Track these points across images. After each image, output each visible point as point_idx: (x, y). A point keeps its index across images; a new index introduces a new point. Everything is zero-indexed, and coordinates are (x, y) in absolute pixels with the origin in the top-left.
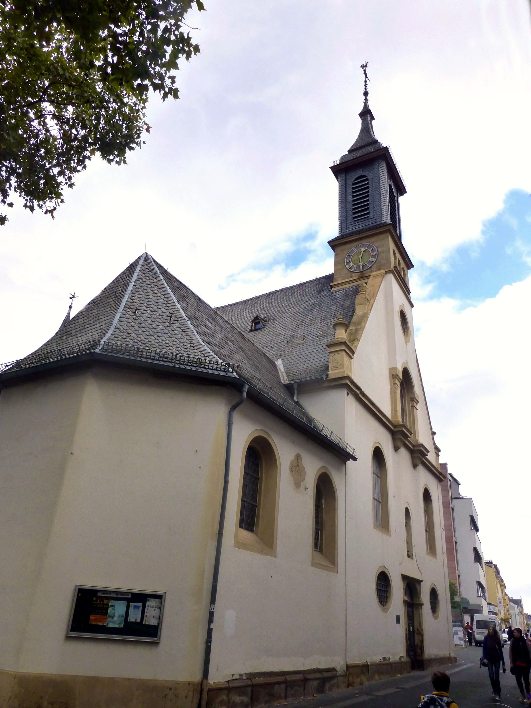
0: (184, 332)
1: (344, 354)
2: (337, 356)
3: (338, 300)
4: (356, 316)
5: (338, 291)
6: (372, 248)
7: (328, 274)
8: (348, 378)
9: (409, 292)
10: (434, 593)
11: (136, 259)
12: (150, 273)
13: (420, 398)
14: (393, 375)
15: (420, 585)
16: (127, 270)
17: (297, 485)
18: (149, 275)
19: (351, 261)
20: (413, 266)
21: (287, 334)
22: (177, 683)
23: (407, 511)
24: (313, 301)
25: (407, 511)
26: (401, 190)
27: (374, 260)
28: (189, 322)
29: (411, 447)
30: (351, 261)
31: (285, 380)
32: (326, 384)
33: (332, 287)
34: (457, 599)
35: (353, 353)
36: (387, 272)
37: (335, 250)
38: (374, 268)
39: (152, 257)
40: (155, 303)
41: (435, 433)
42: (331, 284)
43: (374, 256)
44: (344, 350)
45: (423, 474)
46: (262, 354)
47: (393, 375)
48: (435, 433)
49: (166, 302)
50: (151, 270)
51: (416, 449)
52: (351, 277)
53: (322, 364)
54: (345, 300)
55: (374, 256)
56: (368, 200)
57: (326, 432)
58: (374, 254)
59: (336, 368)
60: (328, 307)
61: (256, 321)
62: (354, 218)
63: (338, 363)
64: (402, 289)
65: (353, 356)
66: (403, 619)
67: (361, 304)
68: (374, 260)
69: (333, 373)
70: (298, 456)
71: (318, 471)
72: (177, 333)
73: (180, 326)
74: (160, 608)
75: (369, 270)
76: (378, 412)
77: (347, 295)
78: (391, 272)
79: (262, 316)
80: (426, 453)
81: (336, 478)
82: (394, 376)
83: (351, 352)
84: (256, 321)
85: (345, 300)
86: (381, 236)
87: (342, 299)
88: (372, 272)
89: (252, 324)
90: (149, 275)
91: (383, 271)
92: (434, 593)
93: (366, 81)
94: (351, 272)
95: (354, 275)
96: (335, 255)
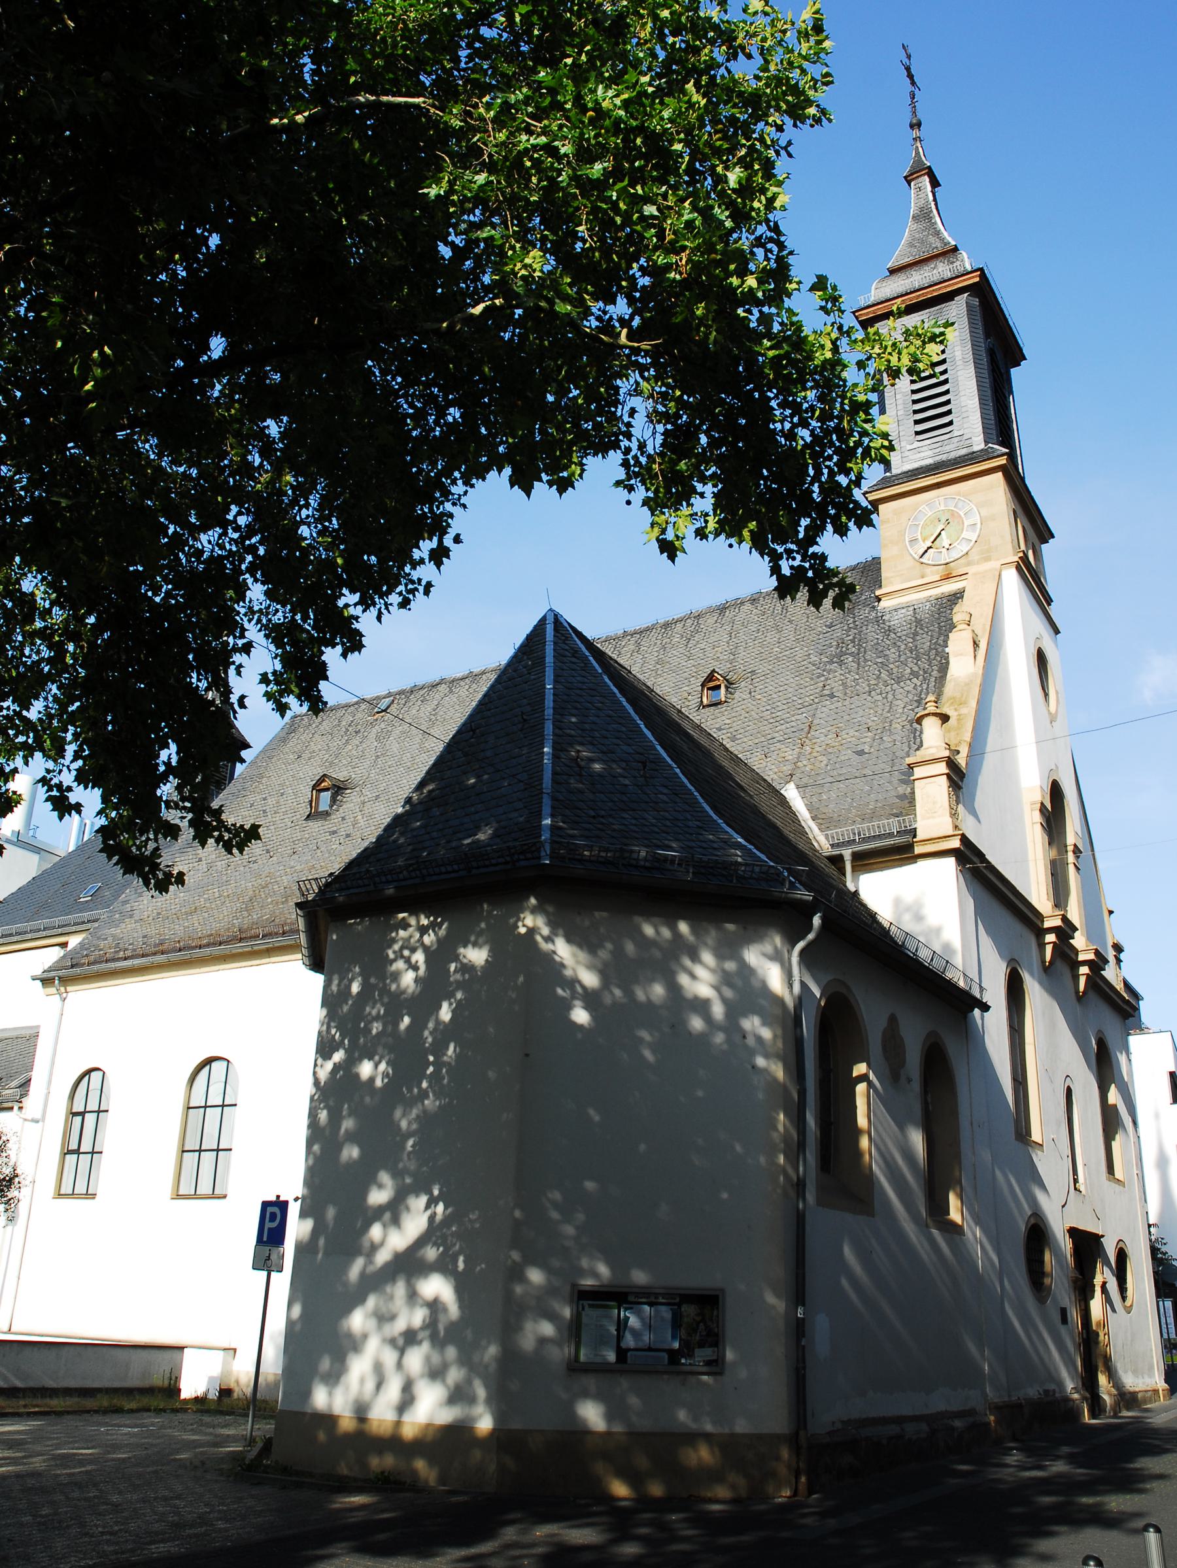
0: (676, 794)
3: (898, 634)
4: (953, 683)
5: (896, 610)
9: (1049, 601)
11: (535, 627)
12: (574, 660)
16: (524, 654)
18: (574, 666)
19: (919, 537)
20: (1052, 536)
21: (793, 719)
26: (1015, 355)
30: (919, 537)
34: (135, 1392)
39: (569, 624)
49: (624, 729)
50: (576, 652)
56: (947, 392)
60: (881, 653)
61: (710, 682)
62: (917, 433)
63: (934, 803)
64: (1031, 591)
65: (962, 781)
67: (961, 655)
70: (893, 1019)
72: (665, 798)
75: (962, 561)
76: (1013, 894)
77: (918, 622)
79: (721, 669)
80: (1070, 932)
81: (952, 1048)
84: (711, 684)
85: (916, 634)
87: (909, 631)
88: (969, 564)
89: (702, 690)
90: (574, 666)
93: (909, 57)
95: (929, 570)
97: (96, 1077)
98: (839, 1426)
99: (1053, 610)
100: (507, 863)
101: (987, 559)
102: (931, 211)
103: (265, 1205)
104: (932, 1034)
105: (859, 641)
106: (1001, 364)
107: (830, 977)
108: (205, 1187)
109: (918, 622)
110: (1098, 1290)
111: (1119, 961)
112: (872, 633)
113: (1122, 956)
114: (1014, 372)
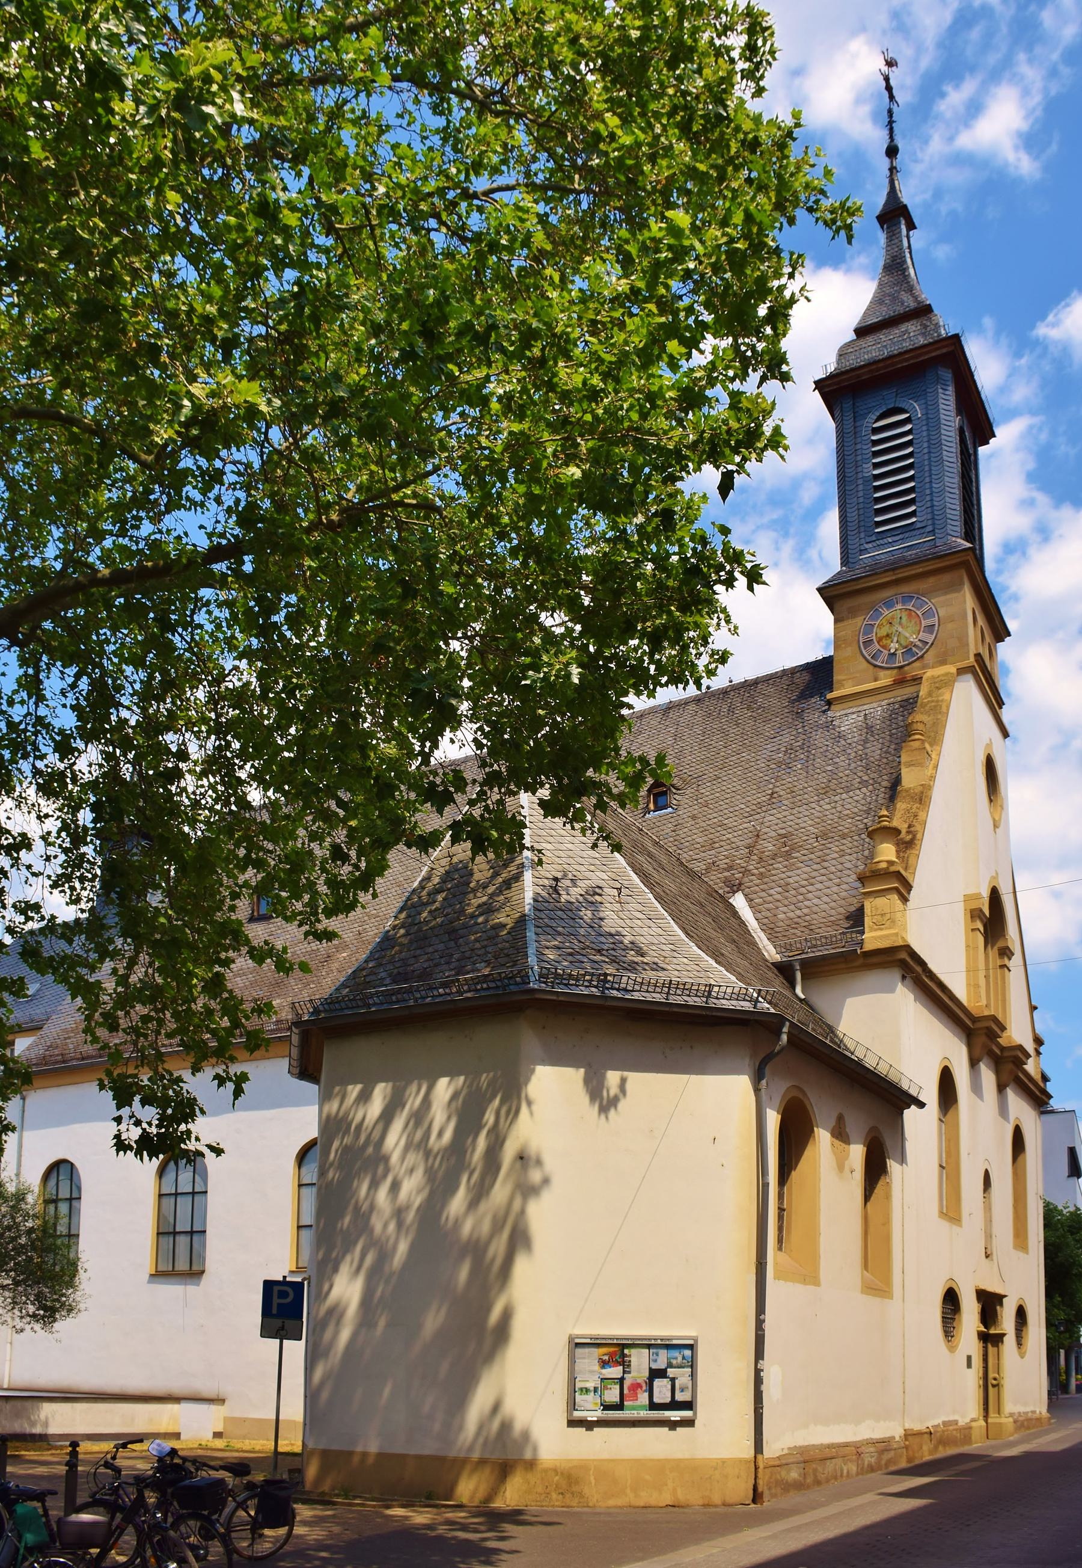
1: (896, 897)
2: (881, 902)
6: (925, 608)
7: (811, 658)
8: (908, 949)
9: (1001, 703)
10: (1021, 1314)
13: (1016, 949)
14: (972, 911)
15: (1001, 1304)
17: (841, 1167)
20: (1009, 635)
22: (724, 1462)
23: (987, 1176)
24: (787, 738)
25: (987, 1176)
27: (930, 638)
28: (651, 896)
29: (998, 1051)
31: (771, 952)
32: (861, 961)
33: (829, 703)
35: (909, 887)
36: (961, 671)
37: (836, 607)
38: (930, 657)
40: (580, 860)
41: (1035, 1008)
42: (829, 696)
43: (930, 628)
44: (896, 889)
45: (1019, 1107)
46: (677, 870)
47: (972, 911)
48: (1035, 1008)
51: (1006, 1054)
52: (876, 680)
53: (841, 910)
54: (866, 741)
55: (930, 628)
57: (870, 1062)
58: (929, 622)
59: (879, 926)
66: (977, 1361)
68: (930, 638)
69: (873, 938)
71: (784, 1096)
73: (640, 908)
74: (692, 1367)
77: (869, 728)
78: (970, 670)
82: (975, 914)
83: (903, 888)
84: (655, 791)
85: (866, 741)
86: (946, 578)
88: (925, 667)
91: (952, 669)
92: (1021, 1314)
94: (875, 666)
96: (836, 621)
97: (63, 1168)
98: (786, 1451)
99: (1006, 714)
100: (497, 987)
101: (943, 662)
102: (905, 262)
103: (194, 1273)
104: (873, 1129)
105: (806, 747)
106: (970, 446)
107: (788, 1084)
108: (182, 1265)
109: (869, 728)
110: (351, 1208)
111: (1038, 1053)
112: (820, 738)
113: (1042, 1049)
114: (982, 450)
